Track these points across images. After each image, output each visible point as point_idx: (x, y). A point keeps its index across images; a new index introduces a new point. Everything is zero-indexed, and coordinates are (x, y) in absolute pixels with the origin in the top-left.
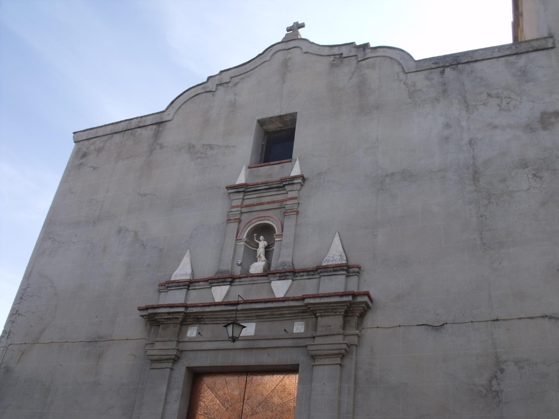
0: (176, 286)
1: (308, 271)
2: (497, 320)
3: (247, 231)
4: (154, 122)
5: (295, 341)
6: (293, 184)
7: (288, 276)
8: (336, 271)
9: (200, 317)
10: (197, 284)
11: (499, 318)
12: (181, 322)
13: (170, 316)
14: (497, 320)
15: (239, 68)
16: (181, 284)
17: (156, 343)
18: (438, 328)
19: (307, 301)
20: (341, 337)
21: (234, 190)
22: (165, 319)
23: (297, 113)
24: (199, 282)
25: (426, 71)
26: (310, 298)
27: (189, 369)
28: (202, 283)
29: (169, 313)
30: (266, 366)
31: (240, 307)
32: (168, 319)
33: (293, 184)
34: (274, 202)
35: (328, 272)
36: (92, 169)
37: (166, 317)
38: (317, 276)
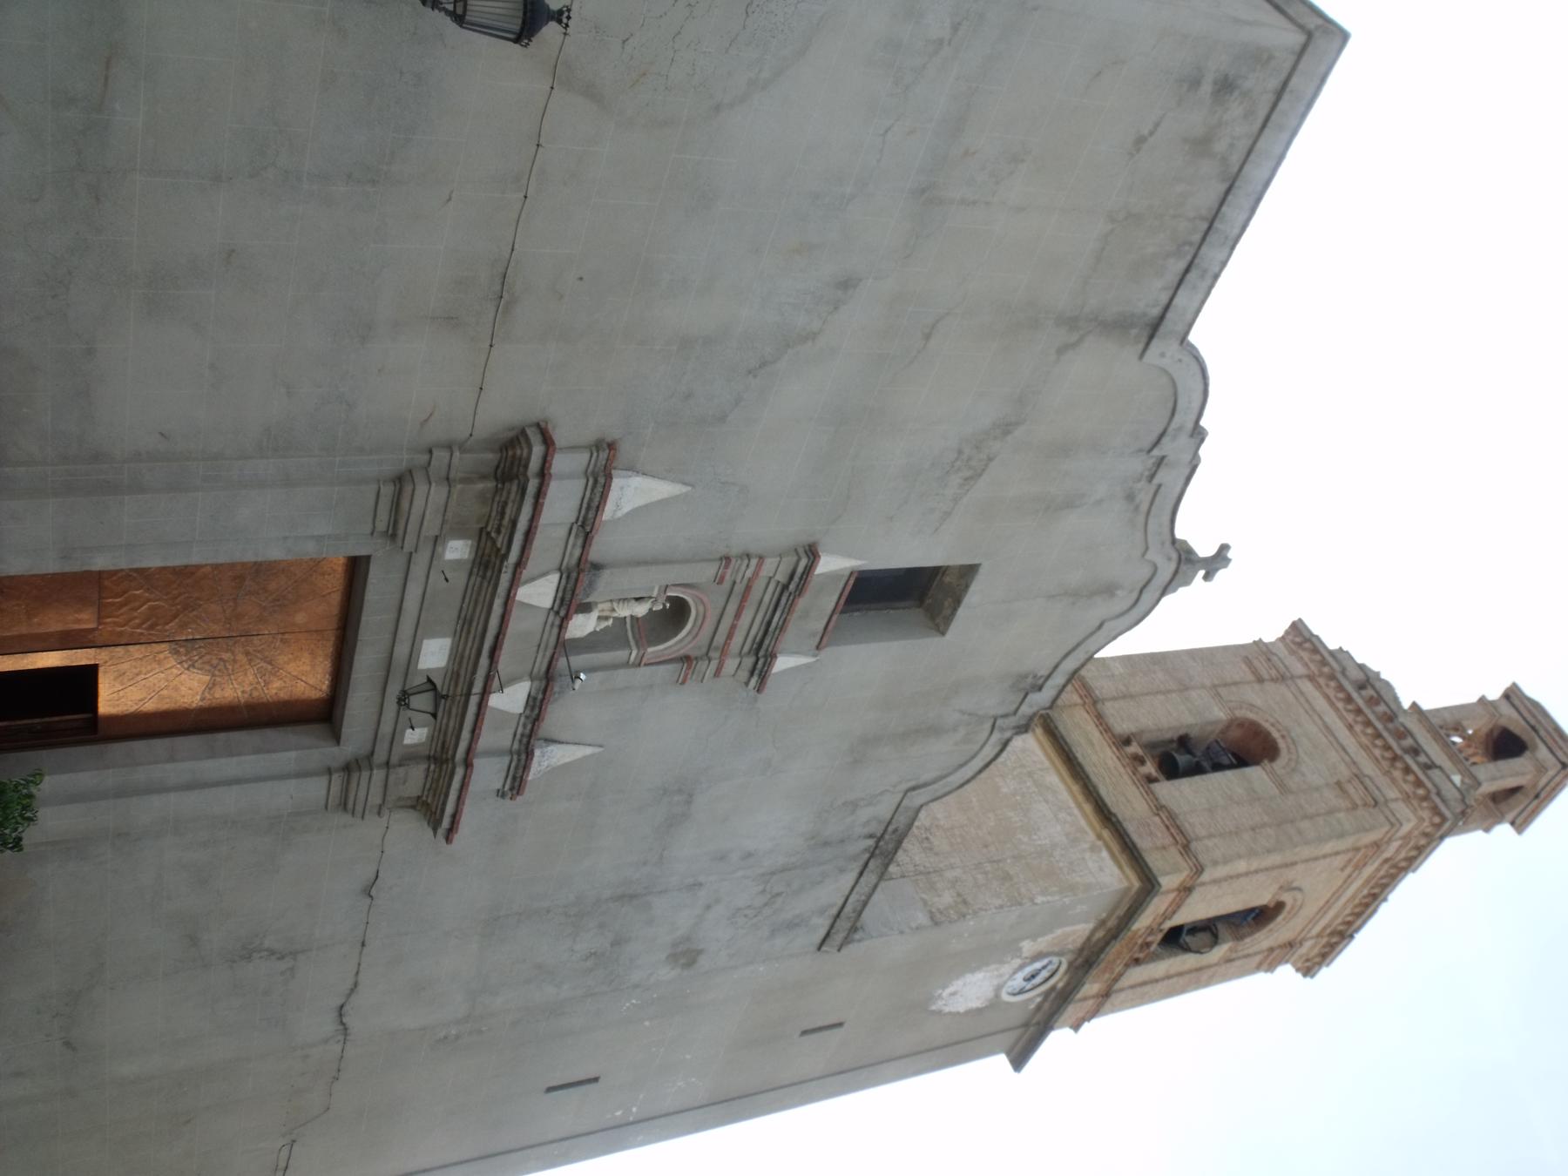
0: (591, 500)
1: (530, 736)
2: (363, 944)
3: (661, 647)
4: (1169, 315)
5: (388, 738)
6: (752, 674)
7: (533, 709)
8: (514, 778)
9: (489, 574)
10: (580, 542)
11: (366, 950)
12: (488, 534)
13: (506, 521)
14: (363, 944)
15: (1173, 502)
16: (591, 515)
17: (445, 490)
18: (368, 892)
19: (460, 772)
20: (378, 801)
21: (800, 570)
22: (506, 503)
23: (969, 571)
24: (583, 547)
25: (1235, 169)
26: (464, 777)
27: (336, 737)
28: (577, 552)
29: (514, 523)
30: (344, 707)
31: (484, 661)
32: (503, 514)
33: (752, 674)
34: (730, 636)
35: (517, 768)
36: (1146, 132)
37: (508, 511)
38: (516, 746)
